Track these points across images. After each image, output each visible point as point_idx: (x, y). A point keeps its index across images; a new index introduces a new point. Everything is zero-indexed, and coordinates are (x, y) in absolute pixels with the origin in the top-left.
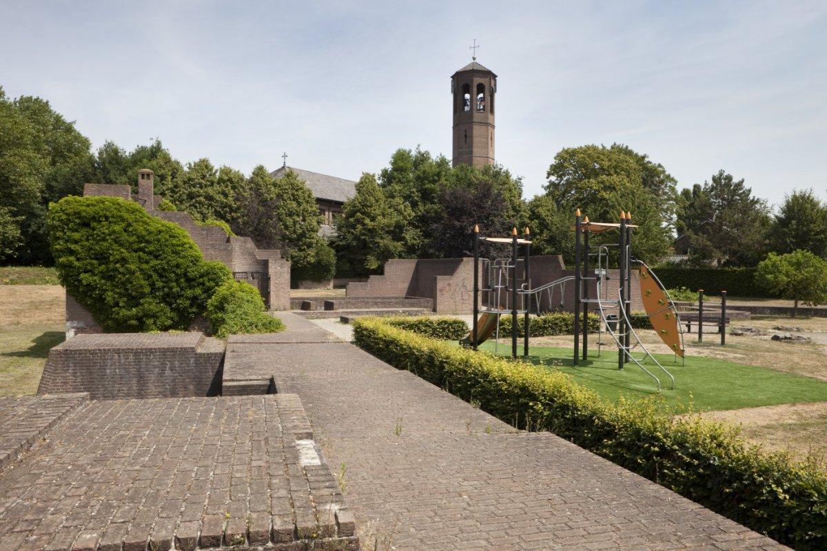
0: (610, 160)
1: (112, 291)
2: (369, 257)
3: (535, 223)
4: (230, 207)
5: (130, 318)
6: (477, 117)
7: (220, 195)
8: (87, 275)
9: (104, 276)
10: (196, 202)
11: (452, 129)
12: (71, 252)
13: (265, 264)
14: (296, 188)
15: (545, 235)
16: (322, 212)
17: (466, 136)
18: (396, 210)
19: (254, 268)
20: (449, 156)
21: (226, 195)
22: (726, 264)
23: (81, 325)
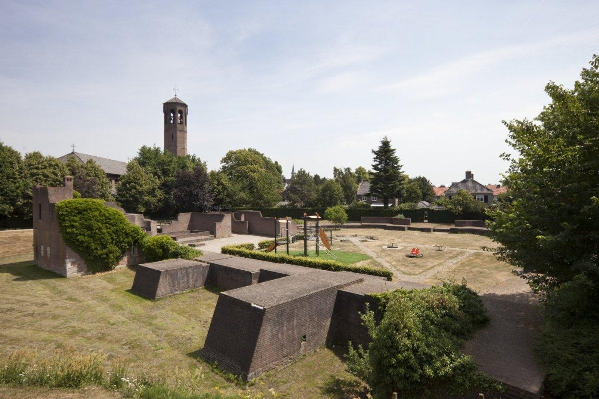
0: (251, 157)
1: (93, 243)
2: (139, 206)
3: (220, 187)
4: (59, 181)
5: (102, 254)
6: (179, 127)
7: (52, 174)
8: (82, 236)
9: (90, 236)
10: (37, 178)
12: (73, 226)
13: (149, 223)
14: (96, 169)
16: (110, 180)
17: (172, 137)
18: (150, 180)
19: (145, 225)
20: (162, 149)
21: (56, 175)
22: (304, 206)
23: (74, 260)
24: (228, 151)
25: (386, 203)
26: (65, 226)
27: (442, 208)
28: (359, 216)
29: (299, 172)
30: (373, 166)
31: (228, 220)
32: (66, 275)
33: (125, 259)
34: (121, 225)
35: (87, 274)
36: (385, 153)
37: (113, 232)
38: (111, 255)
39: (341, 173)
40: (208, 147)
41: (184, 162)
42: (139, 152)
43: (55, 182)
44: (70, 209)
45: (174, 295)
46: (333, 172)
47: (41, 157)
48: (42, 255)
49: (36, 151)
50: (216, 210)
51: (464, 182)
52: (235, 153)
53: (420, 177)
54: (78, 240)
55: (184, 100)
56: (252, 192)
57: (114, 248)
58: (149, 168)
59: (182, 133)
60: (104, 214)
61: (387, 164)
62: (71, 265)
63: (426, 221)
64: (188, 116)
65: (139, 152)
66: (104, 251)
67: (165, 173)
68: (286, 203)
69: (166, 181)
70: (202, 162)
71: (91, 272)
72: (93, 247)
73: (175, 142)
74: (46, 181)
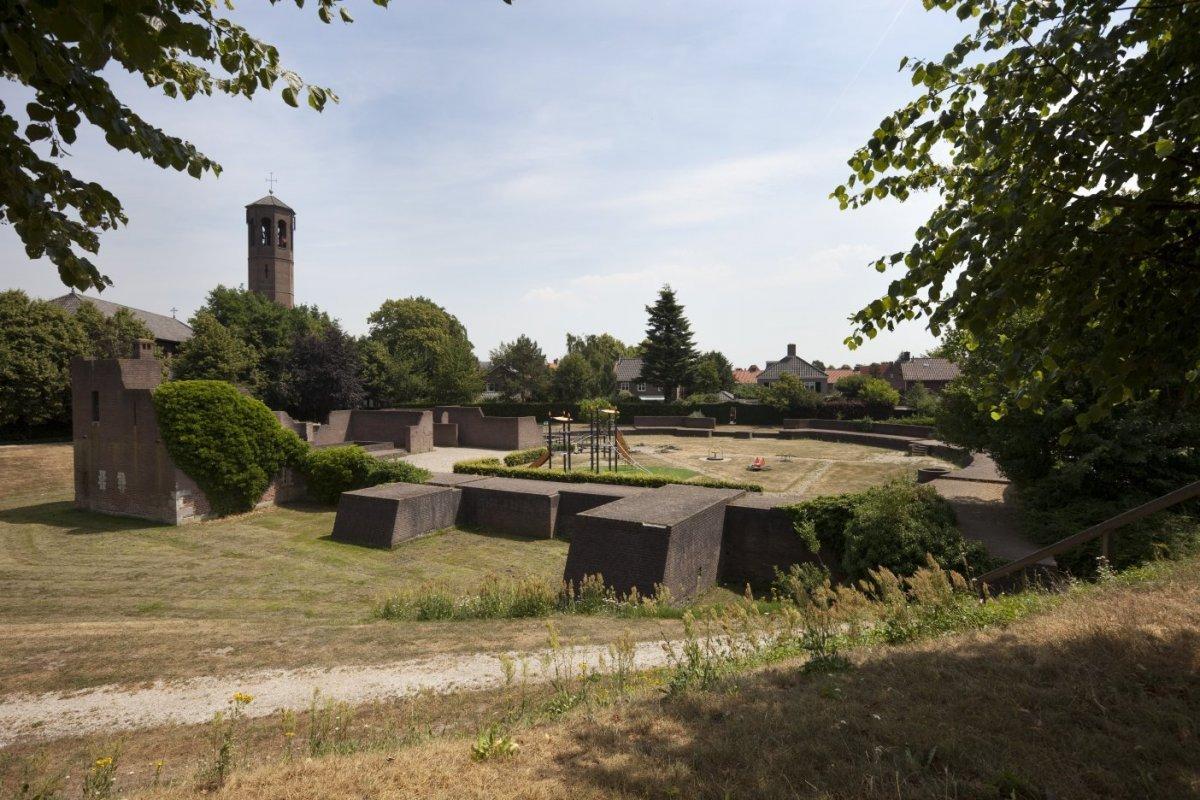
0: (427, 314)
3: (374, 367)
6: (279, 252)
7: (51, 337)
9: (220, 449)
10: (20, 344)
11: (247, 262)
12: (190, 431)
15: (384, 377)
16: (165, 352)
17: (266, 270)
21: (59, 337)
23: (189, 493)
24: (384, 301)
25: (669, 393)
26: (177, 430)
27: (756, 402)
28: (634, 416)
29: (519, 341)
30: (648, 332)
31: (427, 423)
32: (176, 521)
33: (272, 490)
34: (269, 429)
35: (213, 519)
36: (666, 312)
37: (257, 441)
38: (254, 482)
39: (580, 344)
40: (341, 286)
41: (302, 319)
42: (210, 297)
43: (58, 351)
44: (185, 398)
45: (417, 539)
46: (566, 342)
47: (25, 300)
48: (103, 486)
49: (15, 289)
50: (400, 407)
51: (785, 360)
52: (398, 305)
53: (713, 353)
54: (198, 457)
55: (286, 200)
56: (431, 376)
57: (259, 471)
58: (237, 328)
59: (285, 265)
60: (242, 409)
61: (669, 330)
62: (184, 502)
63: (732, 423)
64: (296, 234)
65: (210, 297)
66: (242, 476)
67: (269, 339)
68: (494, 395)
69: (271, 355)
70: (331, 320)
71: (216, 515)
72: (225, 469)
73: (273, 281)
74: (40, 349)
